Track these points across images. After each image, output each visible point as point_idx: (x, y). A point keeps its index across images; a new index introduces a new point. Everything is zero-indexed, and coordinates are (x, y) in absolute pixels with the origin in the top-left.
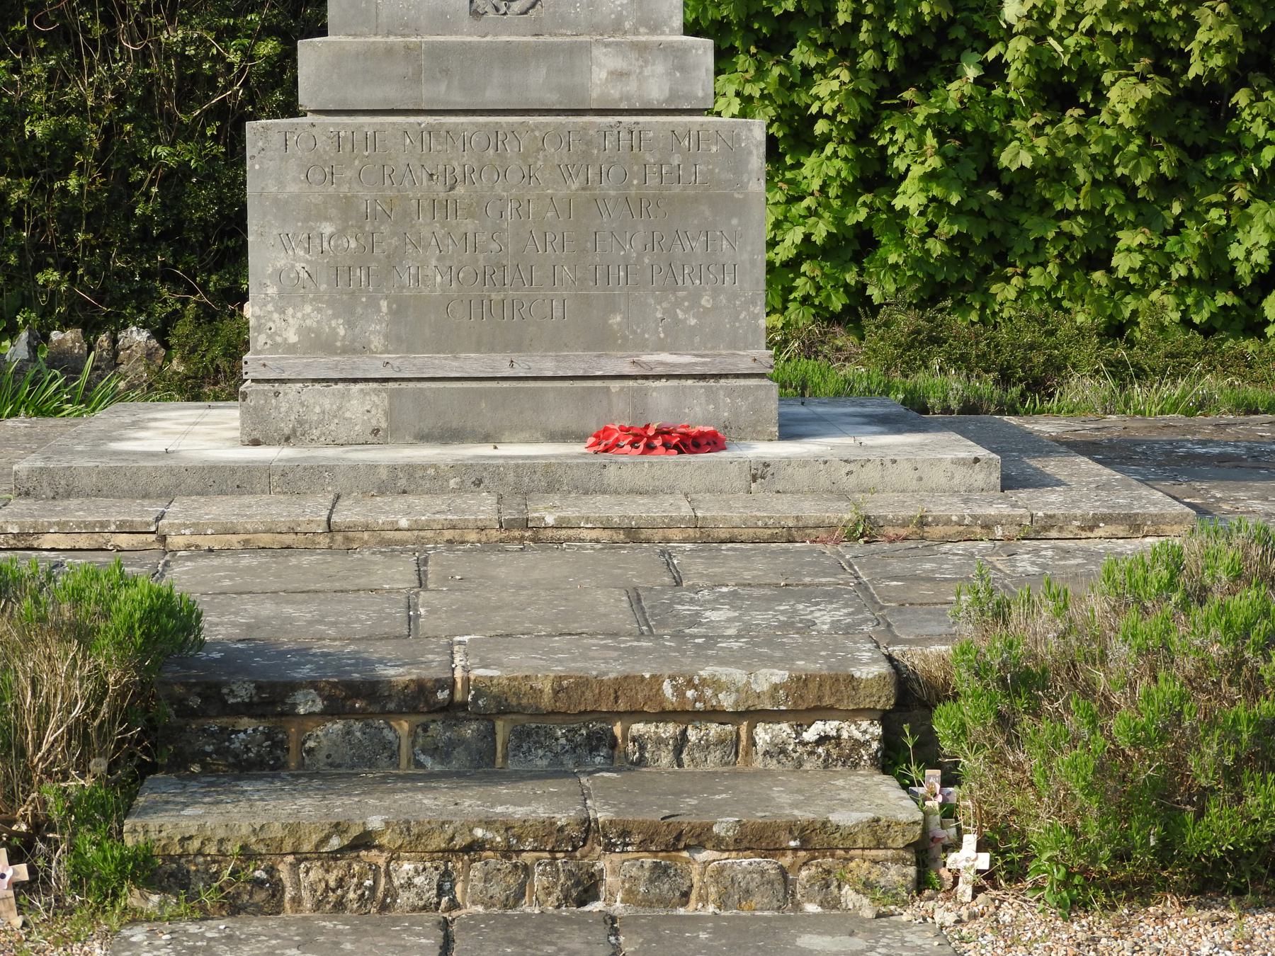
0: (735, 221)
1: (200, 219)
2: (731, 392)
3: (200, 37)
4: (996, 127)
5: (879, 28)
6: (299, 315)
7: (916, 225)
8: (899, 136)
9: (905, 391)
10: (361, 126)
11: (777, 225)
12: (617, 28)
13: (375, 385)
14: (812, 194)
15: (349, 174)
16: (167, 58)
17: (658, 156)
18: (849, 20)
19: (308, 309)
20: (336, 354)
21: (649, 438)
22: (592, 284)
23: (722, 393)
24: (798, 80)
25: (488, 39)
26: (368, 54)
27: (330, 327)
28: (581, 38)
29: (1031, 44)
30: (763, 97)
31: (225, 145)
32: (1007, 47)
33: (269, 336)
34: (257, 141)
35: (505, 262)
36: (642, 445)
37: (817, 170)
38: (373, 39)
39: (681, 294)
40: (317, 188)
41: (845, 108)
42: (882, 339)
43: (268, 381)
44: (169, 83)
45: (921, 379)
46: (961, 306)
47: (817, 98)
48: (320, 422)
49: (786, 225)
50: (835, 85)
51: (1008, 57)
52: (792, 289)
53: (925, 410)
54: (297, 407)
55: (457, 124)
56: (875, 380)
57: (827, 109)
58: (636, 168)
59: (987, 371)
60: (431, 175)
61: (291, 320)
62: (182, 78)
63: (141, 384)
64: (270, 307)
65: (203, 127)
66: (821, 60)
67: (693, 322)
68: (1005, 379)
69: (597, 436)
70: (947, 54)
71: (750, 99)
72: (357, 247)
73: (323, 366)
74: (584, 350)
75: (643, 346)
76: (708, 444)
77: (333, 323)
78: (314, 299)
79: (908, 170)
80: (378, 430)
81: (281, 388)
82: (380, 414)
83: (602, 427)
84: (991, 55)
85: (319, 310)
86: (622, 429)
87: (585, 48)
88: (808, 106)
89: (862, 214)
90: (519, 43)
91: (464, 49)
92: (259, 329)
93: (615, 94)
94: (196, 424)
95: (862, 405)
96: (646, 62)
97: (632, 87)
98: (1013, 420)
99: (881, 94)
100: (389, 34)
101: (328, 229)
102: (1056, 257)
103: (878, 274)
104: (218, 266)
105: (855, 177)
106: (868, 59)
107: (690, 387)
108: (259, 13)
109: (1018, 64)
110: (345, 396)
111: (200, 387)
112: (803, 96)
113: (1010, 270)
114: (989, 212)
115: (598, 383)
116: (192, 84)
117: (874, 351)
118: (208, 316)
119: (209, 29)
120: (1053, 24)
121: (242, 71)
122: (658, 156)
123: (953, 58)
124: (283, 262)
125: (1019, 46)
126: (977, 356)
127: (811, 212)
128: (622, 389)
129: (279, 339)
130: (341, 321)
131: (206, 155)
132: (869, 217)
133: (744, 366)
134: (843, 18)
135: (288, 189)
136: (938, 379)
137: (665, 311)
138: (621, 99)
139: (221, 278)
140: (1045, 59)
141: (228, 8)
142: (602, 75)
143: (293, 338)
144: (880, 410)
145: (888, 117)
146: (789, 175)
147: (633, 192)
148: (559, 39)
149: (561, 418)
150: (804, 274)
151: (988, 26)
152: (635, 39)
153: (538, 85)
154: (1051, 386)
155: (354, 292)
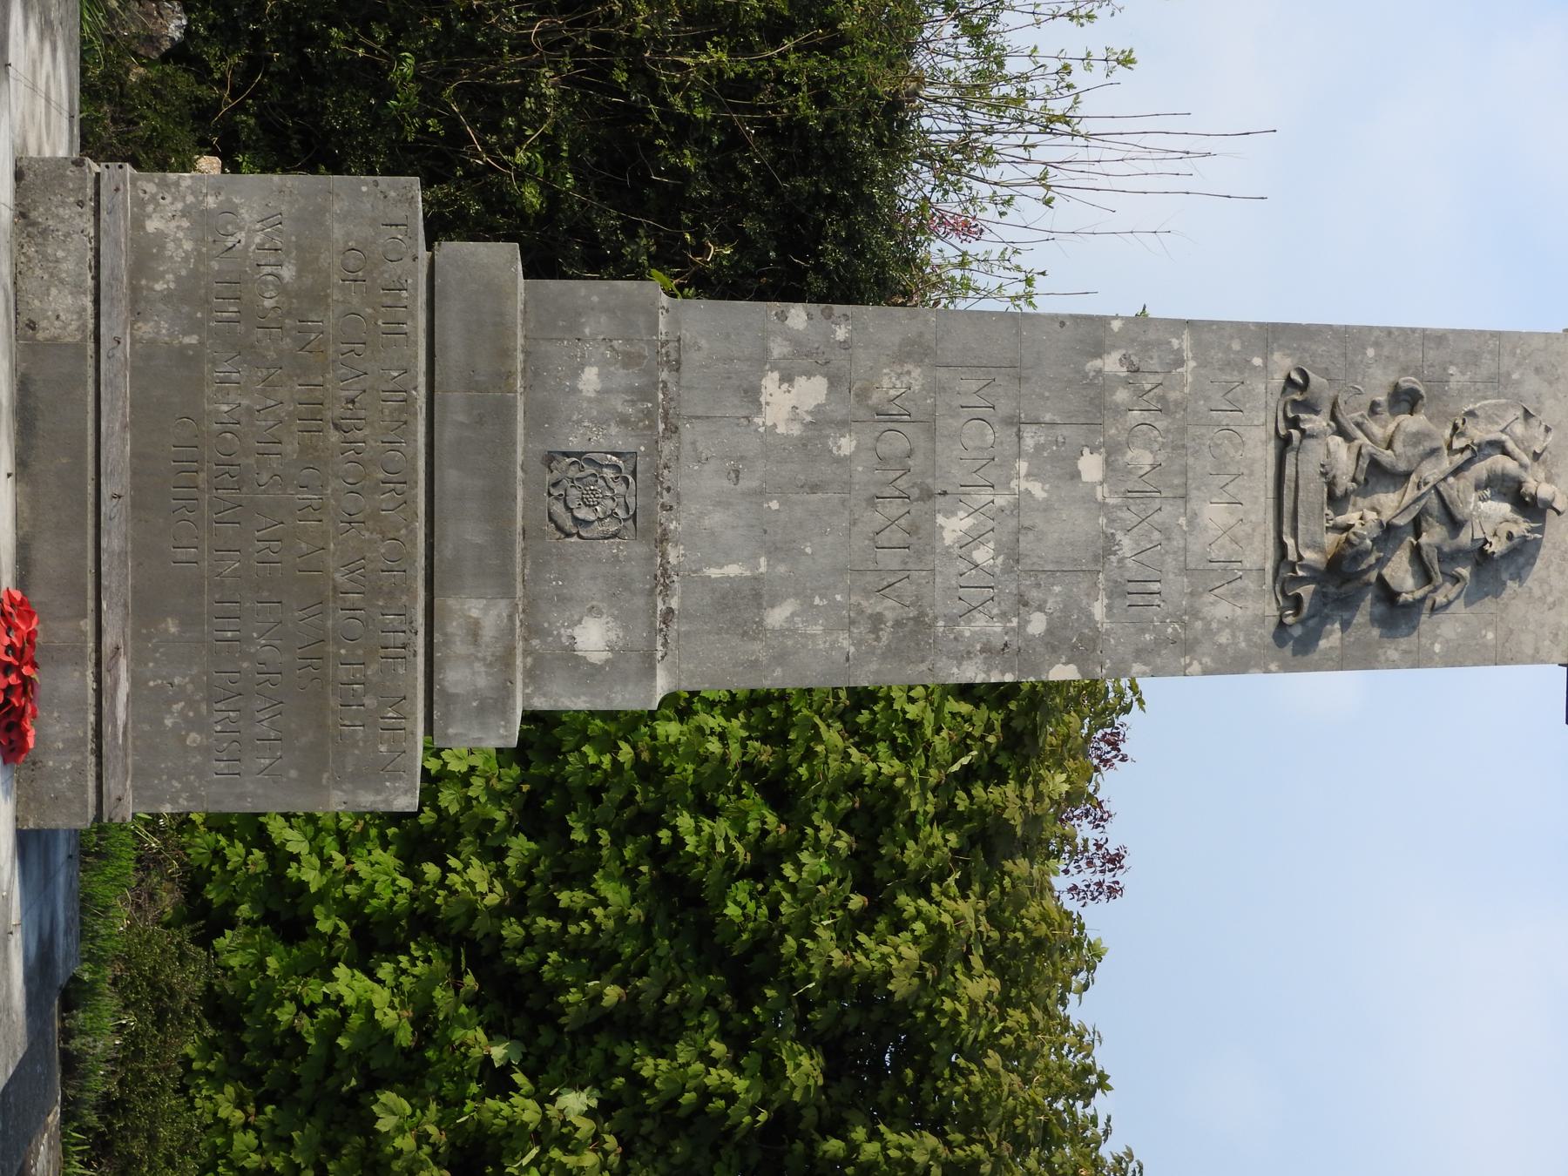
0: (293, 773)
1: (325, 107)
2: (79, 770)
3: (546, 115)
4: (431, 1087)
5: (551, 941)
6: (180, 235)
7: (314, 990)
8: (420, 969)
9: (94, 982)
10: (414, 317)
11: (311, 819)
12: (533, 630)
13: (91, 326)
14: (349, 862)
15: (355, 301)
16: (522, 74)
17: (375, 679)
18: (562, 905)
19: (188, 246)
20: (131, 278)
21: (19, 668)
22: (217, 597)
23: (78, 758)
24: (488, 843)
25: (520, 473)
26: (502, 328)
27: (165, 272)
28: (519, 586)
29: (531, 1127)
30: (469, 799)
31: (416, 140)
32: (527, 1097)
33: (153, 198)
34: (396, 189)
35: (244, 489)
36: (10, 659)
37: (379, 868)
38: (520, 334)
39: (204, 707)
40: (338, 261)
41: (453, 899)
42: (163, 951)
43: (97, 193)
44: (491, 75)
45: (109, 1001)
46: (210, 1047)
47: (467, 866)
48: (45, 257)
49: (310, 830)
50: (482, 887)
51: (516, 1099)
52: (230, 837)
53: (67, 1006)
54: (63, 228)
55: (415, 433)
56: (108, 944)
57: (453, 878)
58: (360, 652)
59: (121, 1083)
60: (353, 402)
61: (173, 224)
62: (499, 91)
63: (114, 27)
64: (190, 199)
65: (438, 115)
66: (512, 872)
67: (168, 722)
68: (109, 1106)
69: (22, 602)
70: (520, 1024)
71: (468, 785)
72: (265, 308)
73: (116, 262)
74: (133, 587)
75: (138, 660)
76: (11, 742)
77: (170, 277)
78: (199, 253)
79: (380, 982)
80: (33, 329)
81: (88, 210)
82: (54, 332)
83: (35, 608)
84: (519, 1078)
85: (186, 259)
86: (32, 634)
87: (508, 593)
88: (457, 855)
89: (324, 926)
90: (514, 511)
91: (509, 442)
92: (164, 185)
93: (452, 628)
94: (48, 100)
95: (67, 932)
96: (490, 665)
97: (460, 648)
98: (54, 1118)
99: (473, 945)
100: (526, 353)
101: (287, 273)
102: (268, 1165)
103: (252, 946)
104: (265, 125)
105: (370, 916)
106: (512, 931)
107: (85, 719)
108: (575, 187)
109: (506, 1111)
110: (78, 289)
111: (110, 101)
112: (470, 849)
113: (251, 1109)
114: (331, 1083)
115: (91, 604)
116: (490, 104)
117: (148, 941)
118: (202, 113)
119: (556, 127)
120: (555, 1153)
121: (505, 165)
122: (375, 679)
123: (516, 1033)
124: (246, 216)
125: (529, 1113)
126: (140, 1070)
127: (326, 863)
128: (84, 634)
129: (150, 208)
130: (172, 286)
131: (403, 117)
132: (321, 935)
133: (112, 786)
134: (564, 898)
135: (336, 225)
136: (109, 1023)
137: (182, 688)
138: (445, 634)
139: (252, 131)
140: (514, 1144)
141: (581, 150)
142: (476, 610)
143: (152, 226)
144: (60, 954)
145: (444, 957)
146: (373, 832)
147: (331, 648)
148: (518, 555)
149: (46, 555)
150: (249, 853)
151: (554, 1074)
152: (519, 651)
153: (465, 533)
154: (100, 1164)
155: (207, 302)
